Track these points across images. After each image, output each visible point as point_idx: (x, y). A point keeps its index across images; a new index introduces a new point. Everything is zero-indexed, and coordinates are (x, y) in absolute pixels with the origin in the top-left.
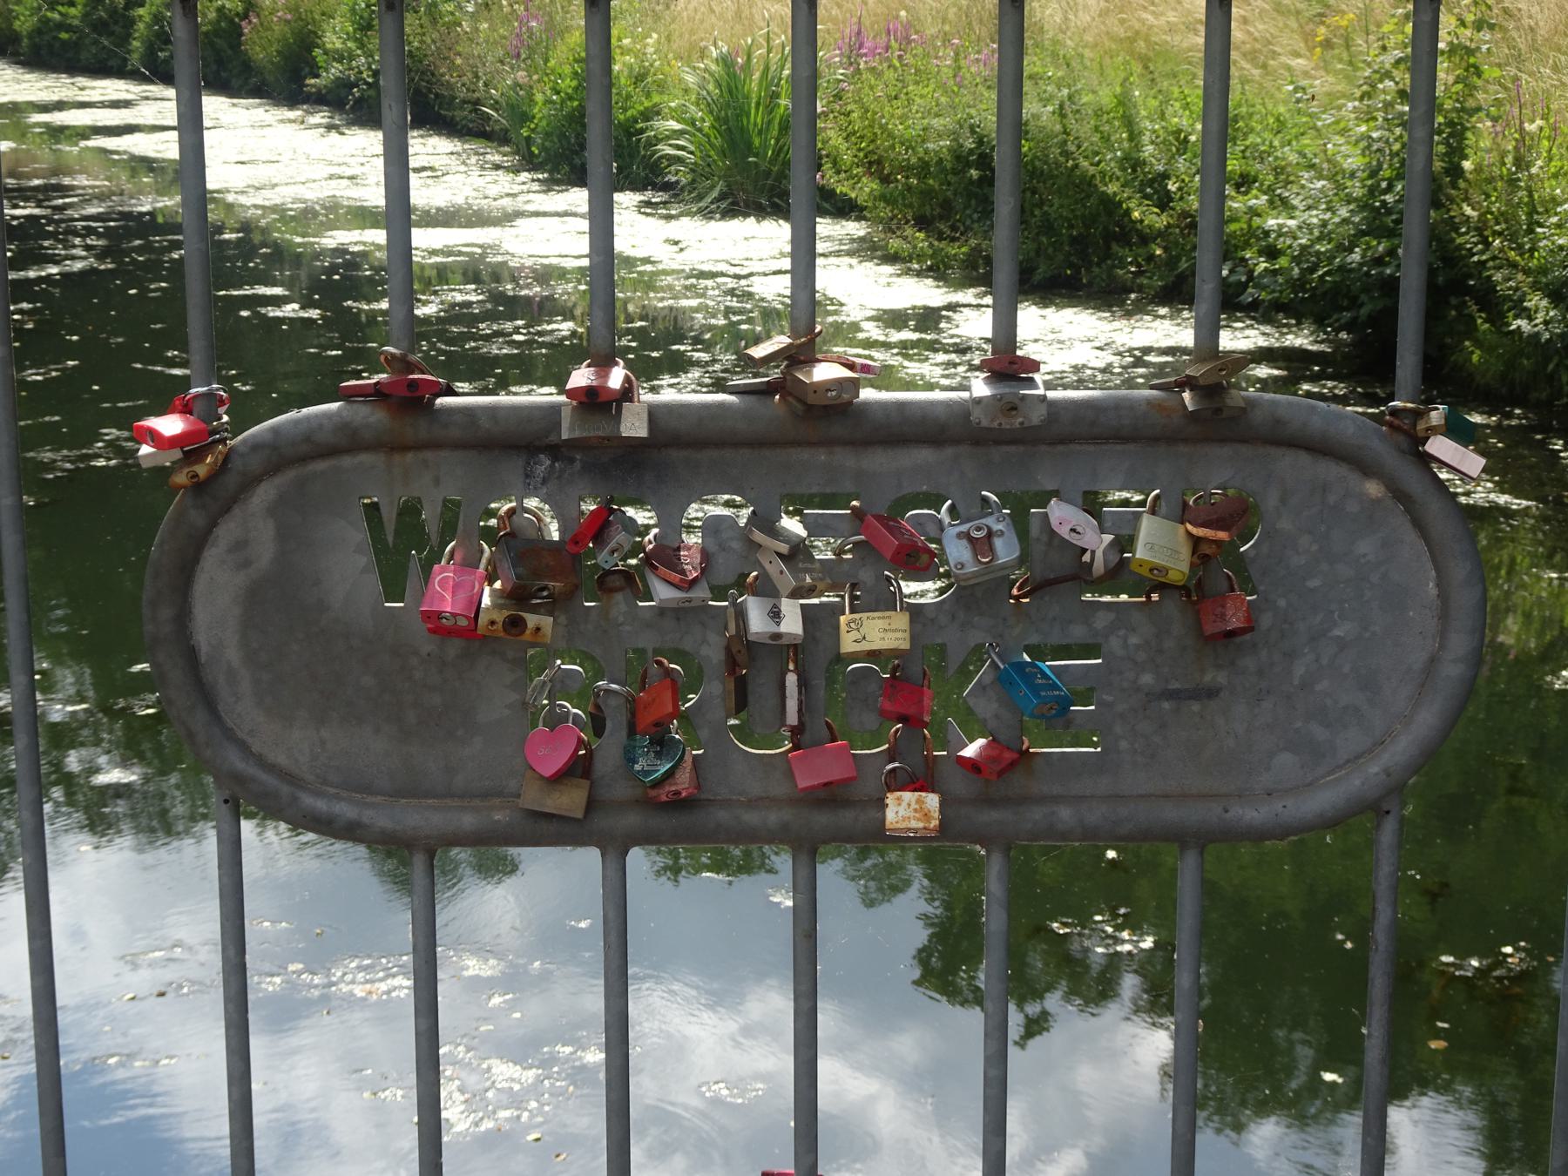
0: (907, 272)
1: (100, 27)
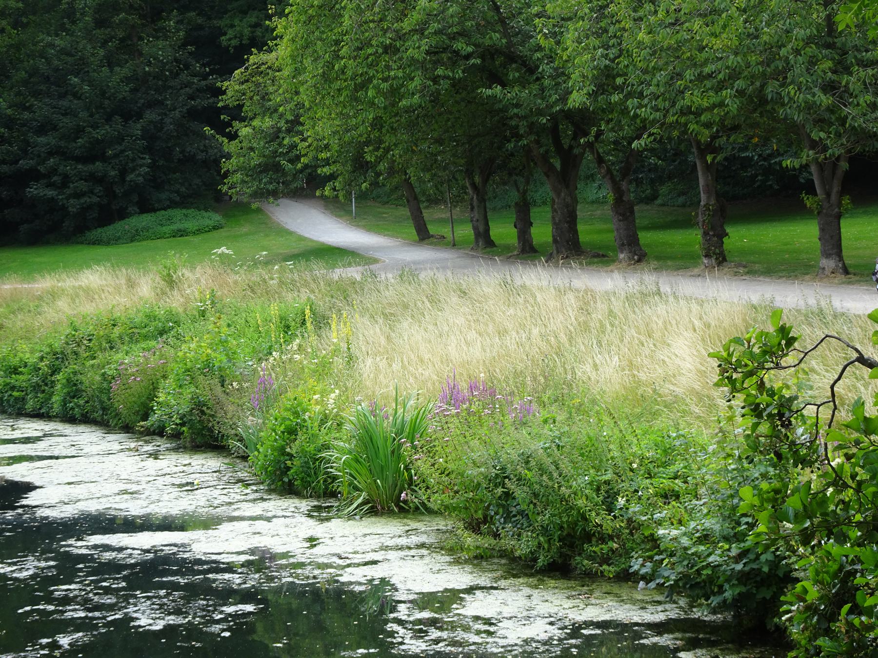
0: (457, 562)
1: (36, 388)
